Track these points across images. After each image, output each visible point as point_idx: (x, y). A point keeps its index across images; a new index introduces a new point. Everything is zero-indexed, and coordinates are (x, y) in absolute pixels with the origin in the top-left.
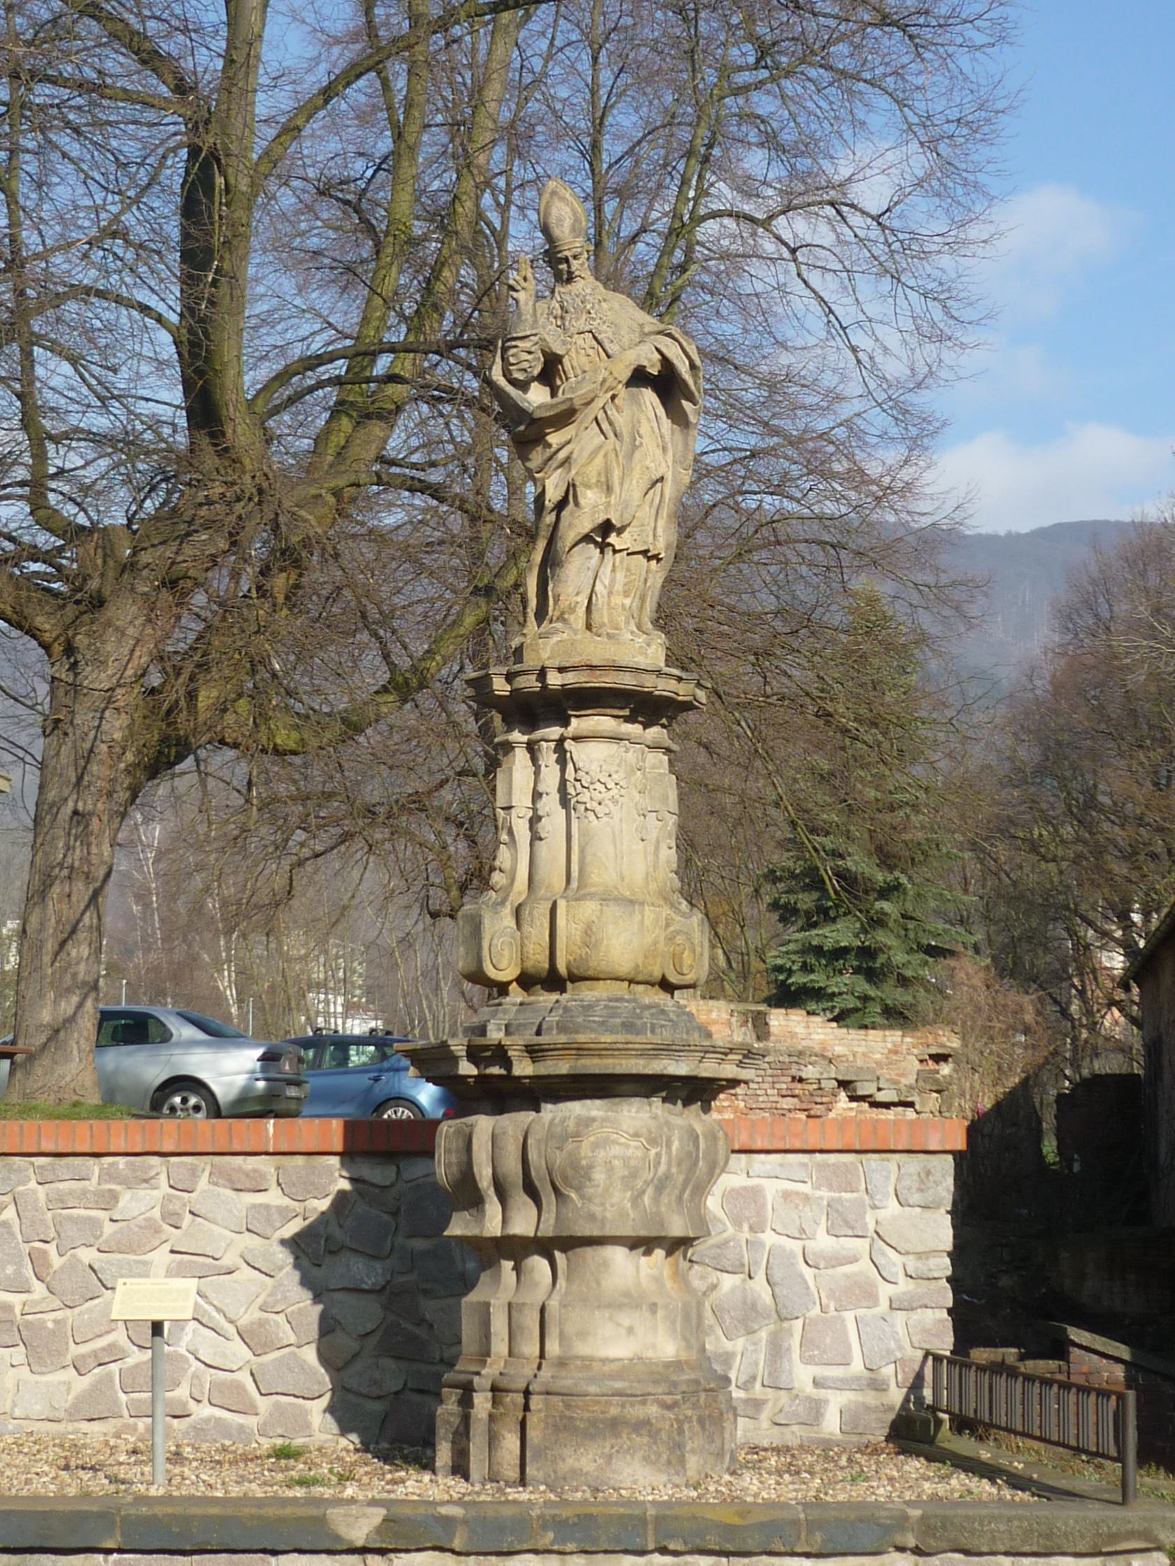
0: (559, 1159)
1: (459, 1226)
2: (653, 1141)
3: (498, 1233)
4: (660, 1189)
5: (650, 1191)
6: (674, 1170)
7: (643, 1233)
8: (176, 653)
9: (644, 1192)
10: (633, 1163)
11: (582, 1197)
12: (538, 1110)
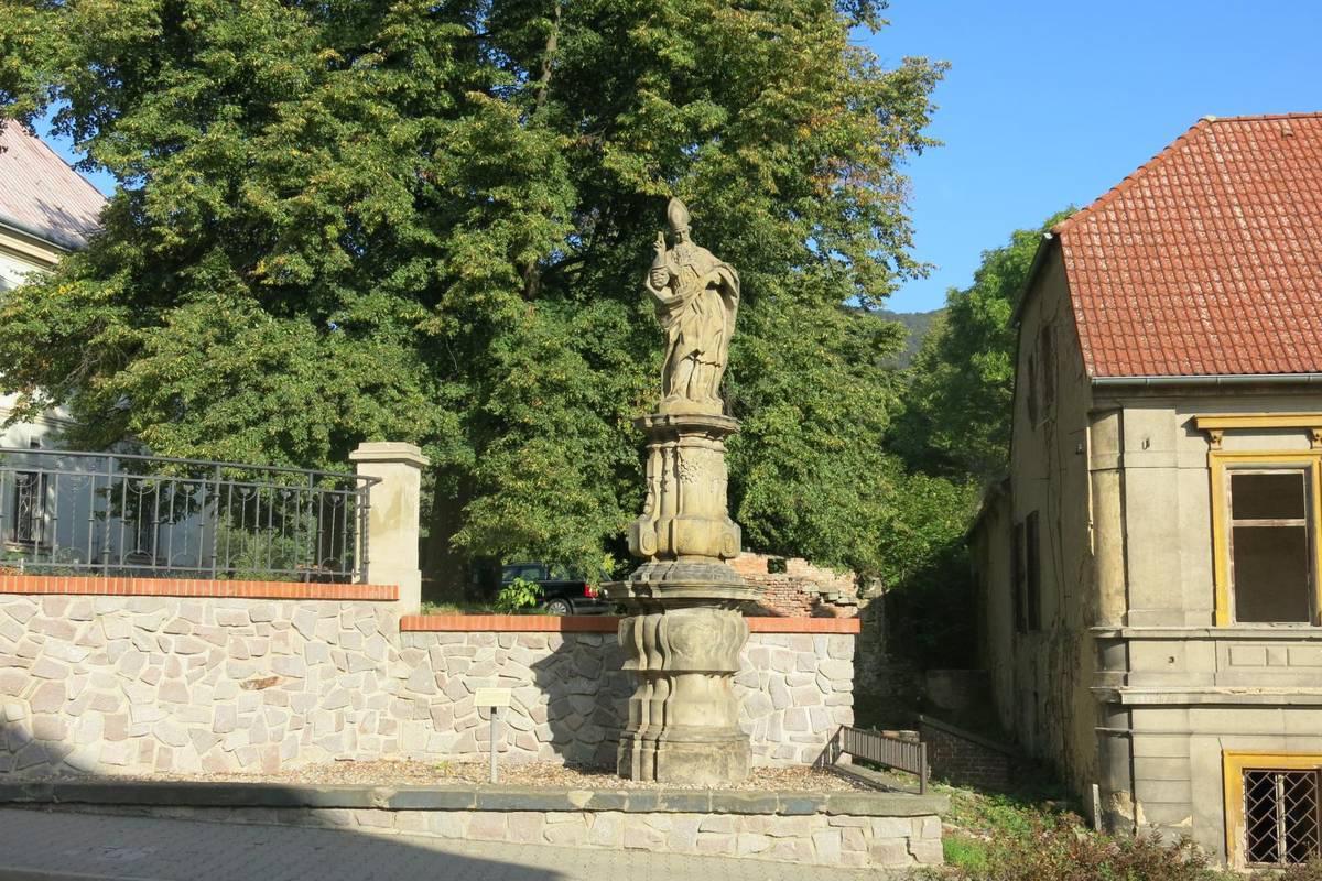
0: (673, 635)
1: (628, 666)
3: (645, 668)
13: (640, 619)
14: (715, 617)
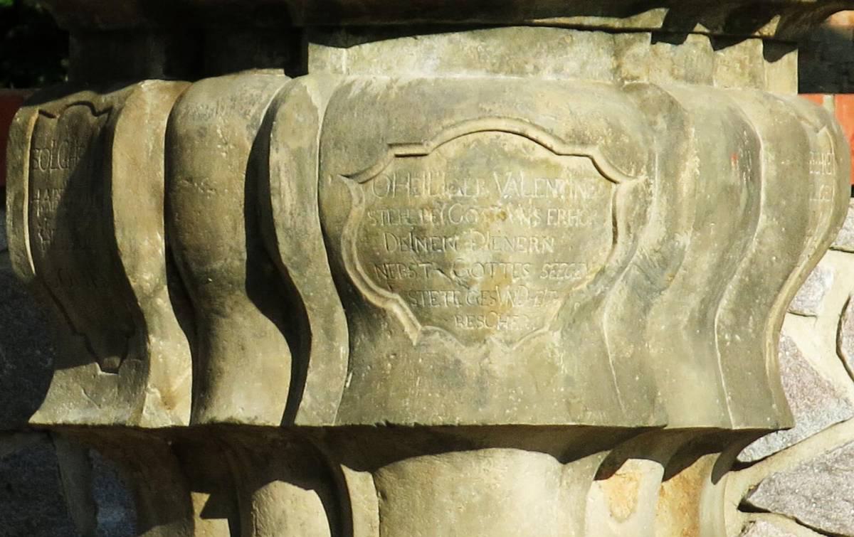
0: (358, 204)
1: (69, 403)
2: (626, 157)
3: (182, 415)
4: (645, 291)
5: (616, 298)
6: (685, 239)
7: (593, 418)
8: (741, 260)
9: (598, 301)
10: (567, 218)
11: (422, 315)
12: (297, 68)
13: (147, 105)
14: (630, 87)
